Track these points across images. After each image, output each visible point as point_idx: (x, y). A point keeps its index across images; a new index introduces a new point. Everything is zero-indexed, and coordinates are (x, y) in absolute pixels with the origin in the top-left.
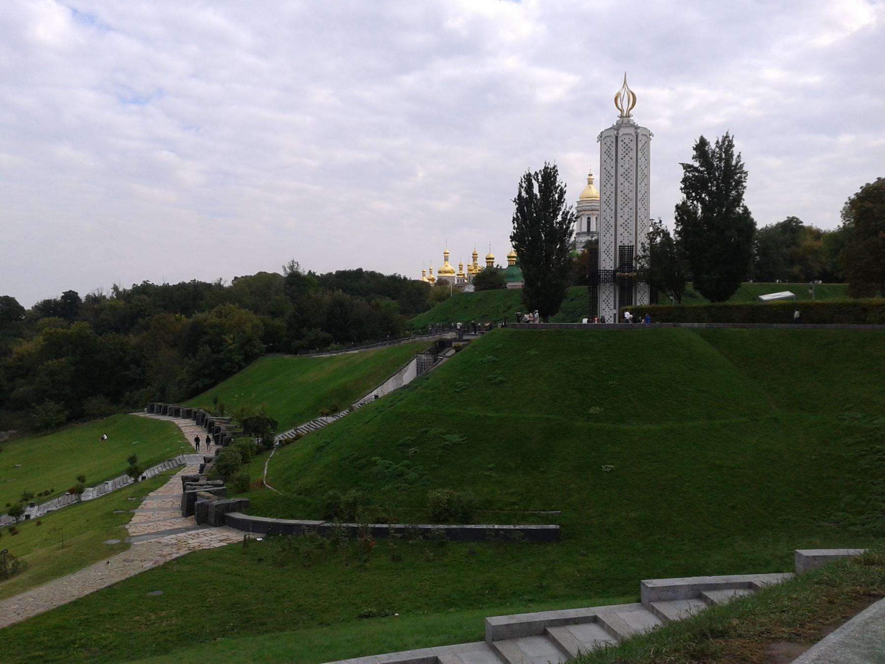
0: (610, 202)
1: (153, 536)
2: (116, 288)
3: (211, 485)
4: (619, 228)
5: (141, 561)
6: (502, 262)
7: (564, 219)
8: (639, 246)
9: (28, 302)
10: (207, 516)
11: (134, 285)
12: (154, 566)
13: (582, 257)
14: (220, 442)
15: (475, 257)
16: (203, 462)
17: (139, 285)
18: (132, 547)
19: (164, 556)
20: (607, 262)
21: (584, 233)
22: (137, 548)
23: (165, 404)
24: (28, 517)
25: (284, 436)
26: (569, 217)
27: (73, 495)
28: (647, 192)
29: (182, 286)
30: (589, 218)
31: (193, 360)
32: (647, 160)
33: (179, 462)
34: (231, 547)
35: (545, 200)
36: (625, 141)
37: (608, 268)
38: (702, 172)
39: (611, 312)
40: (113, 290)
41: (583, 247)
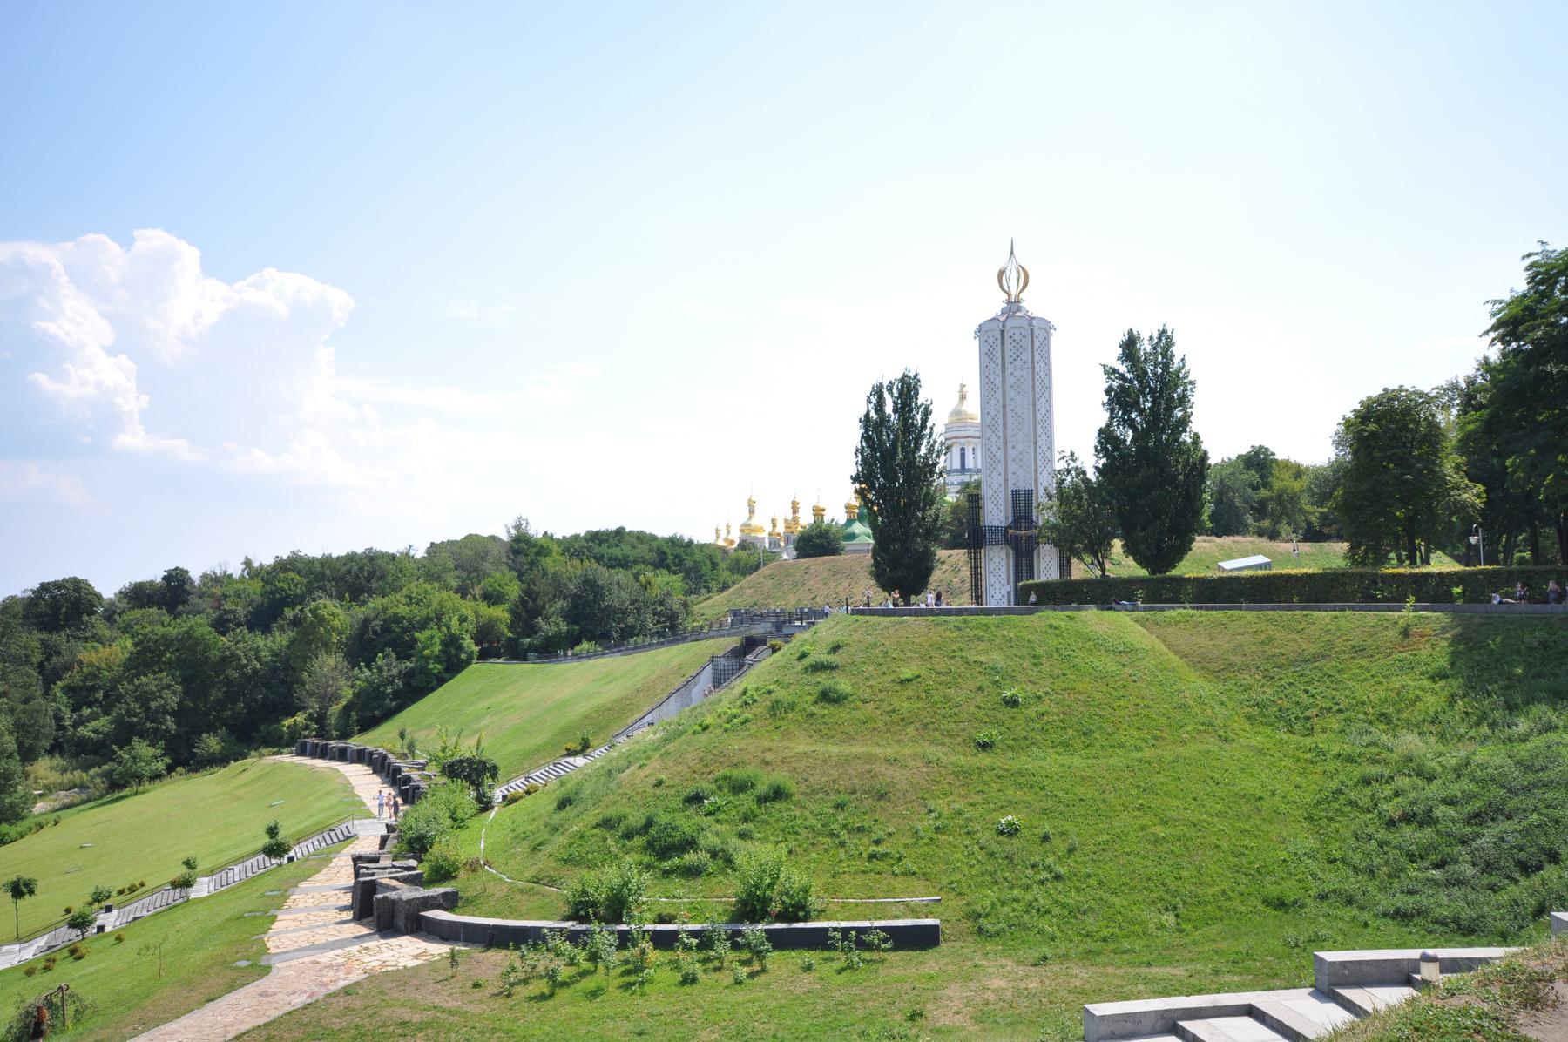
1: (309, 952)
2: (248, 563)
3: (399, 868)
4: (1010, 463)
5: (289, 994)
6: (836, 515)
7: (931, 451)
8: (1041, 491)
9: (108, 586)
10: (393, 917)
11: (277, 557)
12: (309, 1001)
13: (955, 509)
14: (410, 800)
15: (795, 507)
16: (384, 832)
17: (284, 558)
18: (274, 971)
19: (324, 985)
20: (996, 514)
21: (956, 471)
22: (283, 973)
23: (325, 742)
24: (101, 929)
25: (510, 789)
26: (936, 449)
27: (178, 890)
28: (1049, 412)
29: (352, 557)
30: (963, 449)
31: (368, 673)
32: (1048, 364)
33: (346, 833)
34: (431, 966)
36: (1014, 337)
37: (996, 523)
38: (1131, 382)
39: (1003, 589)
40: (244, 566)
41: (958, 492)
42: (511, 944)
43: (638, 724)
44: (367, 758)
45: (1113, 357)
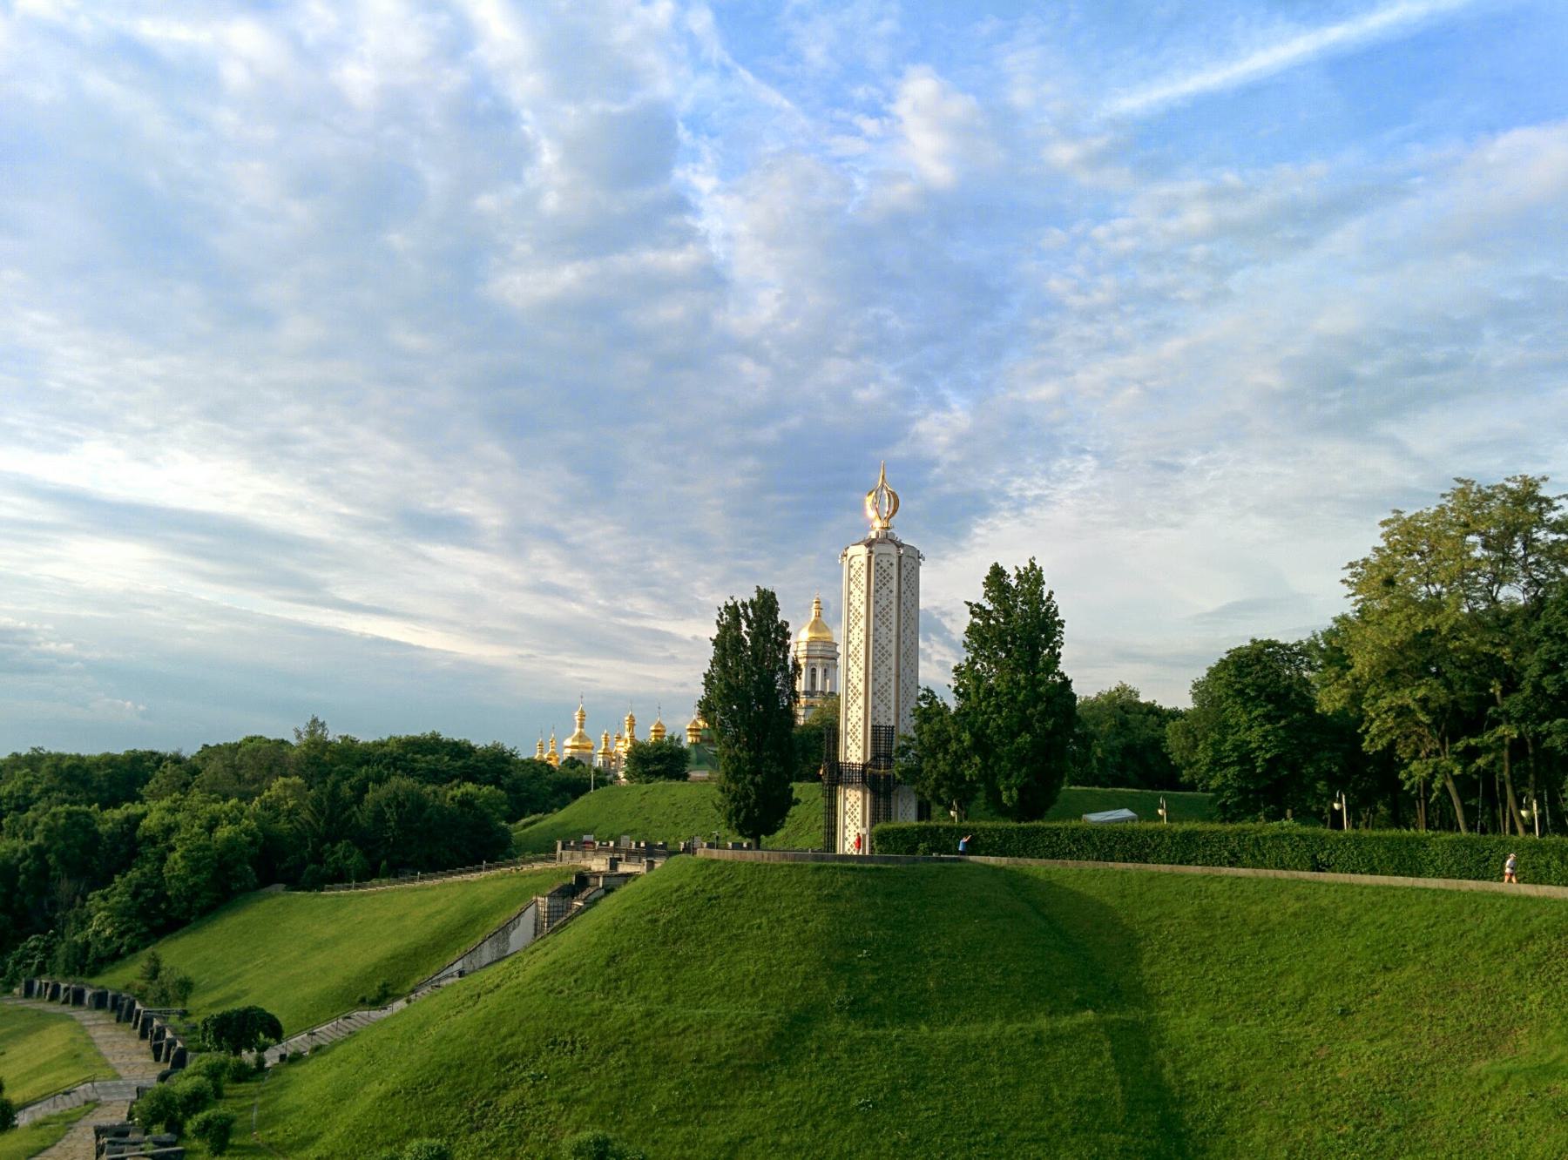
0: (859, 655)
14: (163, 1057)
35: (93, 795)
37: (853, 760)
42: (1289, 812)
43: (445, 973)
44: (109, 1003)
45: (978, 595)
